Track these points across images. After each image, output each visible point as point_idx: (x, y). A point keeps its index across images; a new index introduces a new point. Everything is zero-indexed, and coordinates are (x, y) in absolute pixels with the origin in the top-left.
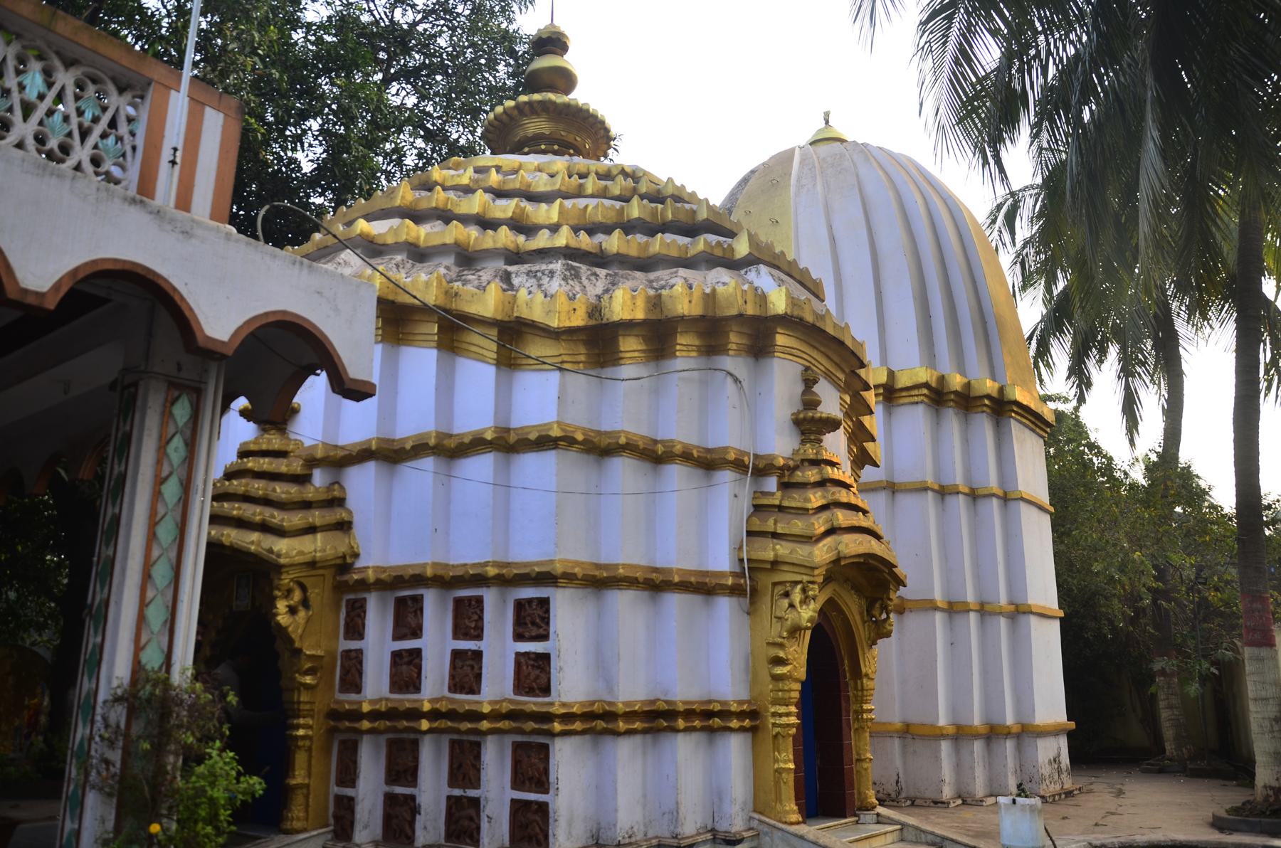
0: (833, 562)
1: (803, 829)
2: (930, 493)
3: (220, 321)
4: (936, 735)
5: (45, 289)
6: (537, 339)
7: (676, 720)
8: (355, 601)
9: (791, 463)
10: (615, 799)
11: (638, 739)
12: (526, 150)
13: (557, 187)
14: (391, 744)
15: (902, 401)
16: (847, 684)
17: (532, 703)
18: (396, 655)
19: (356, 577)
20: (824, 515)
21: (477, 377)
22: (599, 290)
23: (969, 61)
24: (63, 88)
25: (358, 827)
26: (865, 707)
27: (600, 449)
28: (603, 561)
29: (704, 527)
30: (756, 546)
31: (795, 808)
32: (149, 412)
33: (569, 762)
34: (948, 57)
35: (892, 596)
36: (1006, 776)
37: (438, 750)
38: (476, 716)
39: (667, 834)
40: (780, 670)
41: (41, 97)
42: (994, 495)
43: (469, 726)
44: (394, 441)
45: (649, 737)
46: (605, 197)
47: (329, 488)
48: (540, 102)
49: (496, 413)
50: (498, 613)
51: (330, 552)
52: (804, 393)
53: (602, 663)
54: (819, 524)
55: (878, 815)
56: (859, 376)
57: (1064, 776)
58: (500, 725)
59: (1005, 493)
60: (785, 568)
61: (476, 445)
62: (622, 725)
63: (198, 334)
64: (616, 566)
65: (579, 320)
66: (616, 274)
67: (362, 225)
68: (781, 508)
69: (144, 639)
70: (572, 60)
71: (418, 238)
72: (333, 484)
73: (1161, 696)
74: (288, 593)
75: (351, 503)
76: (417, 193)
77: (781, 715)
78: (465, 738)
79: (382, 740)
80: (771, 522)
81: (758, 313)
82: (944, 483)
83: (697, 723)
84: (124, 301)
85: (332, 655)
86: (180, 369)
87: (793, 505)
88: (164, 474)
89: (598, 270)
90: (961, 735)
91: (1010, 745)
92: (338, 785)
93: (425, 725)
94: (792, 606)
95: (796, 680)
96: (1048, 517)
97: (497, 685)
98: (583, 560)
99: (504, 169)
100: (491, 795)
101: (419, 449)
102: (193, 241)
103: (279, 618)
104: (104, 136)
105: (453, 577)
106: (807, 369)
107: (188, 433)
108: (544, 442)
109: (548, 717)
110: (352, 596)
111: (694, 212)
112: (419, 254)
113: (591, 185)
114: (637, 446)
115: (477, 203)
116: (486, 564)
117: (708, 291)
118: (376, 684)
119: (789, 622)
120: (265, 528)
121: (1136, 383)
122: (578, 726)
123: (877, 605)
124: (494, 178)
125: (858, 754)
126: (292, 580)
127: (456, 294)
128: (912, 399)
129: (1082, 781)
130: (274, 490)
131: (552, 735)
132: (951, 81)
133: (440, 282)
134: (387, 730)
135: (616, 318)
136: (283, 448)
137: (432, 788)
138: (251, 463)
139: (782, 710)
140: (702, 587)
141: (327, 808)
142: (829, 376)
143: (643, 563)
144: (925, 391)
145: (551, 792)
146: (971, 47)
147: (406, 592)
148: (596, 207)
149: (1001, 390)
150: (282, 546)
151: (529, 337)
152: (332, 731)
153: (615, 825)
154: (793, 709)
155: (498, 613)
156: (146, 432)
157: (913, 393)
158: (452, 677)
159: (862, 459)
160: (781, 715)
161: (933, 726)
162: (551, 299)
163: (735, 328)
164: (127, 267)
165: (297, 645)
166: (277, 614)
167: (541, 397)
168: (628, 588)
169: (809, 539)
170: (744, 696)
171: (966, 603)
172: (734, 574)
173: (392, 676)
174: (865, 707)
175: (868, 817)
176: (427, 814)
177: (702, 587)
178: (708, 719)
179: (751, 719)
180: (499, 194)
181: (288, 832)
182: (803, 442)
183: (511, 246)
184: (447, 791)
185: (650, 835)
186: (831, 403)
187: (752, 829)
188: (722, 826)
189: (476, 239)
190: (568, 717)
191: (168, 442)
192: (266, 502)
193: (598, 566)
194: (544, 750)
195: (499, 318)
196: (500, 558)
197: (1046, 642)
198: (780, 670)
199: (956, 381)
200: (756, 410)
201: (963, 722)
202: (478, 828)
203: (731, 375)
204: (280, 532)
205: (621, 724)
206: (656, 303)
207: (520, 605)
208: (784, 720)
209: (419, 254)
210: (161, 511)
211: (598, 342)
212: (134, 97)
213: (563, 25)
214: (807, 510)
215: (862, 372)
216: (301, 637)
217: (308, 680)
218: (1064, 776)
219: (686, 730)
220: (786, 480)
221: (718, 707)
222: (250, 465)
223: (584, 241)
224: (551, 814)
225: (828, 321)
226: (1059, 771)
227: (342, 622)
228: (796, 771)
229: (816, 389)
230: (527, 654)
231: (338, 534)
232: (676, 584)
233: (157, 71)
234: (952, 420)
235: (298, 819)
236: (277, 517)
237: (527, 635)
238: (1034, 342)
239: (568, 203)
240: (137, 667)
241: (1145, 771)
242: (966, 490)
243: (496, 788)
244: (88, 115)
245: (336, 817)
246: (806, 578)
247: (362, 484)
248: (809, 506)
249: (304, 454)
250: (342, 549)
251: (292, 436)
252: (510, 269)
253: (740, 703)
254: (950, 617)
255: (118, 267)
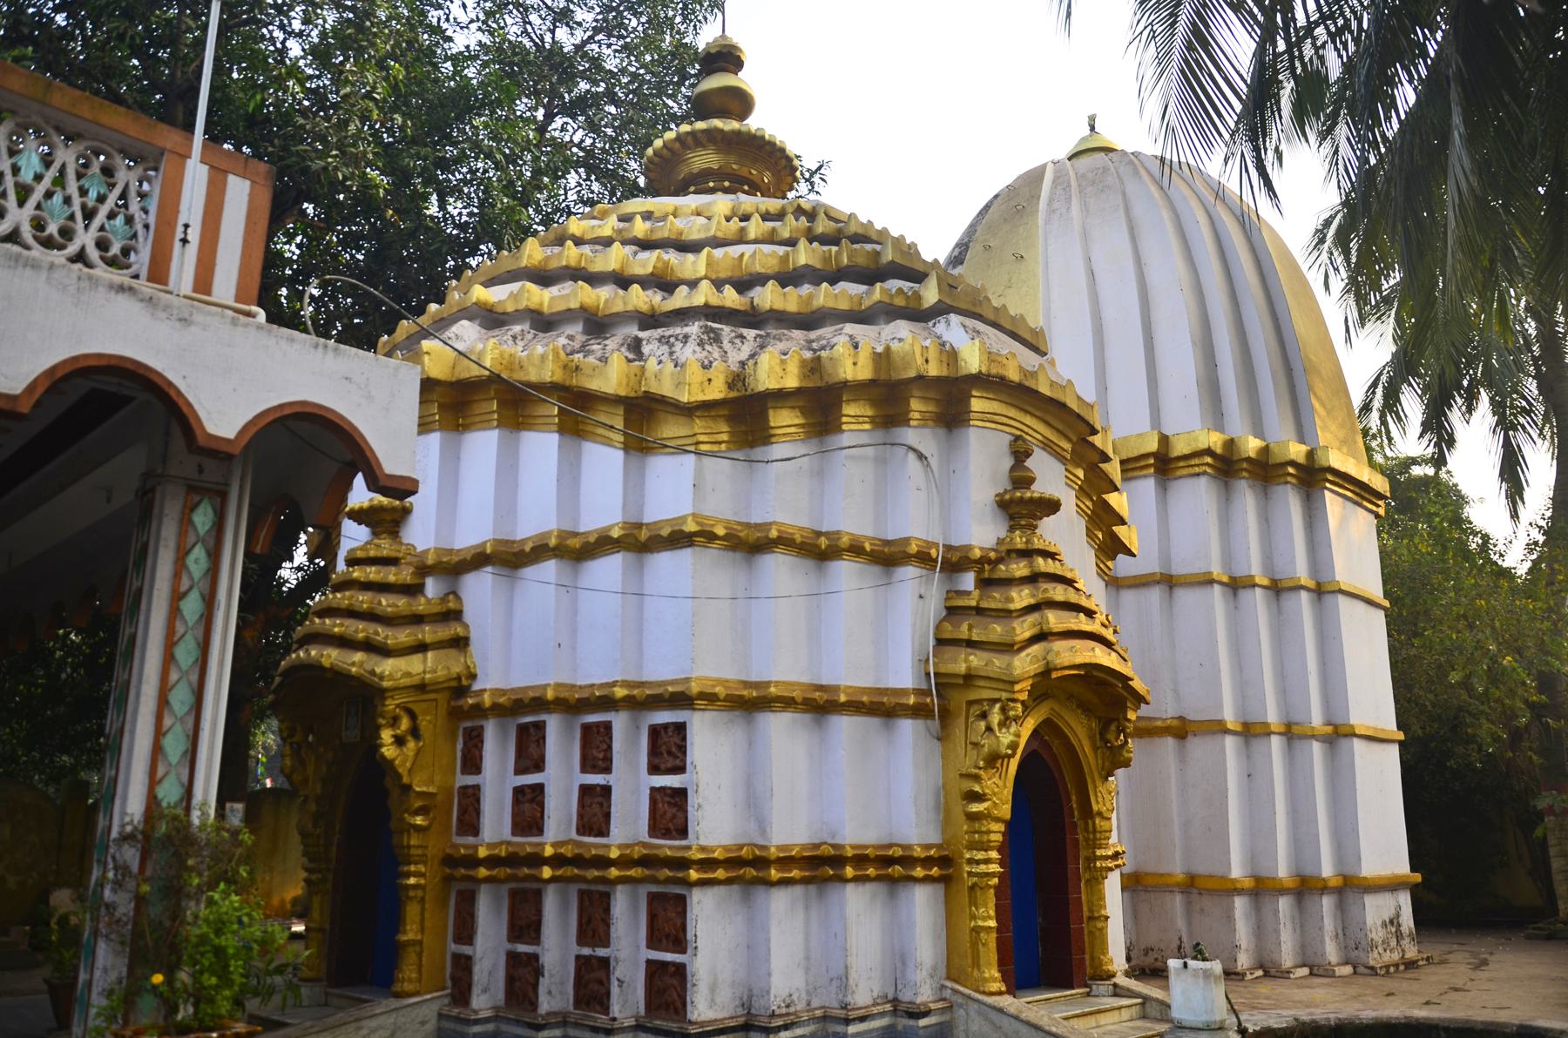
0: (1042, 674)
1: (1007, 1002)
2: (1217, 587)
3: (224, 415)
4: (1230, 890)
5: (18, 391)
6: (670, 417)
7: (844, 867)
8: (473, 729)
9: (992, 555)
10: (768, 961)
11: (798, 890)
12: (692, 189)
13: (712, 233)
14: (513, 894)
15: (1179, 473)
16: (1075, 825)
17: (667, 847)
18: (519, 792)
19: (470, 701)
20: (1031, 618)
21: (604, 461)
22: (744, 356)
23: (1205, 45)
24: (63, 166)
25: (476, 990)
26: (1098, 853)
27: (750, 544)
28: (754, 678)
29: (880, 634)
30: (946, 656)
31: (997, 975)
32: (165, 520)
33: (711, 917)
34: (1178, 41)
35: (1132, 715)
36: (1323, 942)
37: (634, 908)
38: (604, 862)
39: (835, 1004)
40: (976, 807)
41: (38, 178)
42: (1303, 587)
43: (596, 873)
44: (514, 542)
45: (812, 888)
46: (772, 242)
47: (444, 599)
48: (704, 131)
49: (624, 506)
50: (629, 741)
51: (441, 673)
52: (1012, 469)
53: (753, 800)
54: (1024, 629)
55: (1115, 985)
56: (1093, 445)
57: (1406, 942)
58: (631, 873)
59: (1319, 584)
60: (982, 683)
61: (602, 545)
62: (774, 874)
63: (198, 432)
64: (768, 684)
65: (717, 392)
66: (768, 335)
67: (479, 293)
68: (979, 611)
69: (161, 771)
70: (747, 79)
71: (541, 304)
72: (447, 594)
73: (1552, 841)
74: (394, 722)
75: (468, 616)
76: (549, 251)
77: (978, 862)
78: (593, 887)
79: (504, 890)
80: (965, 627)
81: (945, 373)
82: (1238, 574)
83: (871, 871)
84: (109, 404)
85: (448, 792)
86: (201, 471)
87: (993, 606)
88: (183, 588)
89: (745, 331)
90: (1261, 889)
91: (1327, 903)
92: (455, 942)
93: (547, 872)
94: (989, 729)
95: (998, 820)
96: (1382, 613)
97: (629, 825)
98: (729, 677)
99: (657, 214)
100: (622, 955)
101: (540, 551)
102: (193, 329)
103: (384, 750)
104: (112, 216)
105: (579, 700)
106: (1017, 438)
107: (212, 542)
108: (678, 539)
109: (684, 864)
110: (468, 724)
111: (877, 254)
112: (544, 322)
113: (755, 228)
114: (793, 540)
115: (615, 258)
116: (614, 684)
117: (880, 349)
118: (496, 825)
119: (986, 749)
120: (369, 646)
121: (1520, 438)
122: (720, 874)
123: (1113, 727)
124: (640, 228)
125: (1091, 911)
126: (398, 706)
127: (577, 368)
128: (1191, 470)
129: (1436, 949)
130: (380, 603)
131: (691, 885)
132: (1182, 71)
133: (556, 355)
134: (509, 879)
135: (761, 388)
136: (393, 554)
137: (557, 946)
138: (357, 573)
139: (980, 855)
140: (880, 707)
141: (444, 968)
142: (1047, 446)
143: (805, 679)
144: (1209, 460)
145: (689, 951)
146: (1207, 26)
147: (526, 714)
148: (753, 255)
149: (1311, 455)
150: (387, 666)
151: (662, 415)
152: (448, 880)
153: (768, 992)
154: (994, 854)
155: (629, 741)
156: (162, 543)
157: (1193, 462)
158: (580, 816)
159: (1111, 547)
160: (978, 862)
161: (1224, 878)
162: (689, 369)
163: (916, 393)
164: (113, 362)
165: (405, 780)
166: (382, 745)
167: (677, 486)
168: (784, 710)
169: (1008, 648)
170: (934, 838)
171: (1266, 724)
172: (918, 692)
173: (514, 815)
174: (1098, 853)
175: (1103, 987)
176: (551, 976)
177: (880, 707)
178: (888, 867)
179: (942, 867)
180: (646, 245)
181: (398, 995)
182: (1012, 529)
183: (644, 308)
184: (575, 950)
185: (815, 1004)
186: (1050, 477)
187: (944, 999)
188: (906, 996)
189: (607, 301)
190: (708, 864)
191: (188, 553)
192: (372, 616)
193: (747, 685)
194: (681, 901)
195: (623, 393)
196: (632, 677)
197: (1379, 777)
198: (976, 807)
199: (1252, 445)
200: (948, 493)
201: (1265, 873)
202: (608, 994)
203: (914, 450)
204: (385, 652)
205: (773, 872)
206: (814, 367)
207: (656, 732)
208: (983, 868)
209: (544, 322)
210: (180, 629)
211: (745, 416)
212: (146, 170)
213: (736, 36)
214: (1010, 612)
215: (1097, 440)
216: (410, 771)
217: (419, 820)
218: (1406, 942)
219: (856, 879)
220: (986, 575)
221: (899, 852)
222: (355, 574)
223: (730, 298)
224: (689, 977)
225: (1041, 378)
226: (1399, 936)
227: (459, 754)
228: (999, 930)
229: (1029, 463)
230: (662, 789)
231: (453, 652)
232: (843, 704)
233: (168, 137)
234: (1246, 497)
235: (410, 980)
236: (382, 633)
237: (663, 766)
238: (1379, 391)
239: (719, 253)
240: (152, 800)
241: (1529, 937)
242: (1266, 582)
243: (629, 947)
244: (93, 194)
245: (453, 978)
246: (1004, 695)
247: (479, 590)
248: (1012, 606)
249: (414, 560)
250: (457, 669)
251: (405, 541)
252: (642, 335)
253: (928, 847)
254: (1247, 744)
255: (103, 362)
